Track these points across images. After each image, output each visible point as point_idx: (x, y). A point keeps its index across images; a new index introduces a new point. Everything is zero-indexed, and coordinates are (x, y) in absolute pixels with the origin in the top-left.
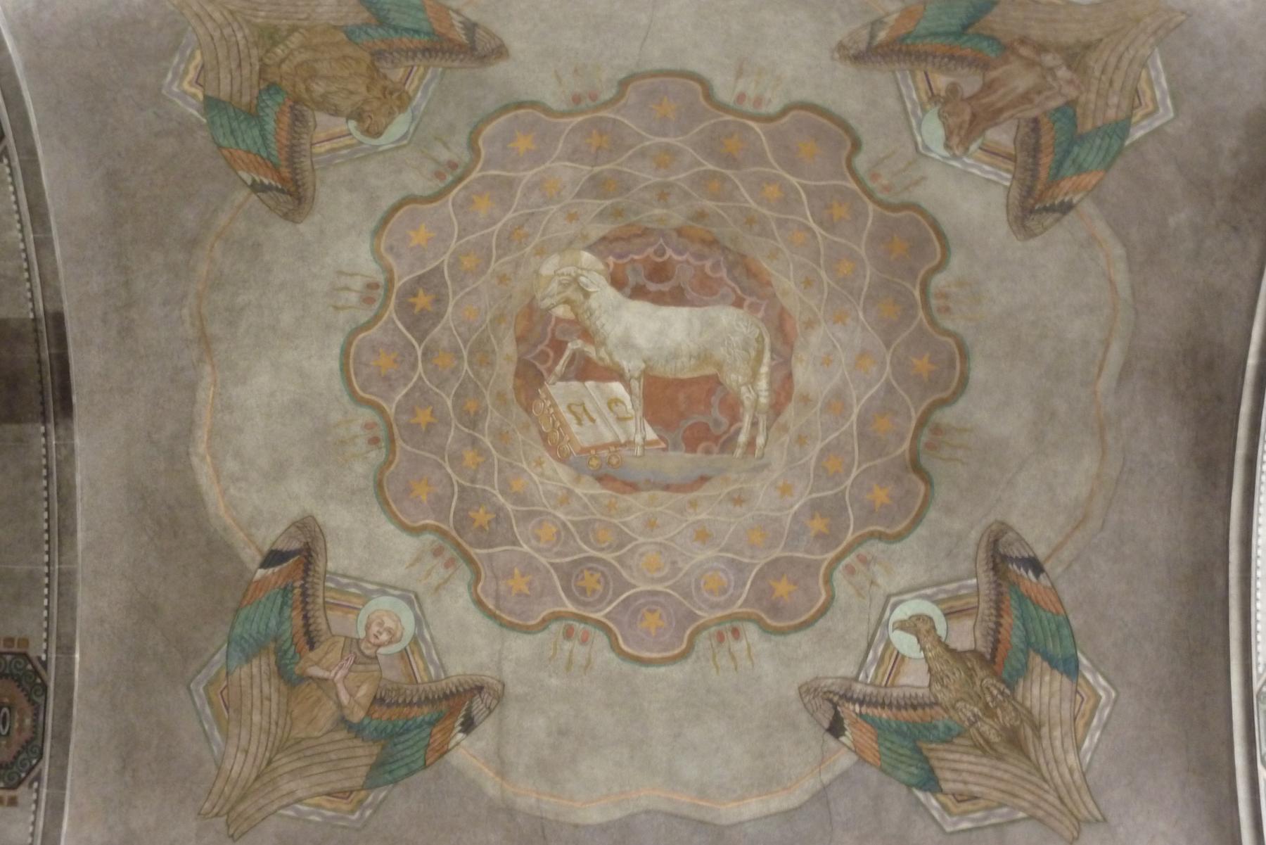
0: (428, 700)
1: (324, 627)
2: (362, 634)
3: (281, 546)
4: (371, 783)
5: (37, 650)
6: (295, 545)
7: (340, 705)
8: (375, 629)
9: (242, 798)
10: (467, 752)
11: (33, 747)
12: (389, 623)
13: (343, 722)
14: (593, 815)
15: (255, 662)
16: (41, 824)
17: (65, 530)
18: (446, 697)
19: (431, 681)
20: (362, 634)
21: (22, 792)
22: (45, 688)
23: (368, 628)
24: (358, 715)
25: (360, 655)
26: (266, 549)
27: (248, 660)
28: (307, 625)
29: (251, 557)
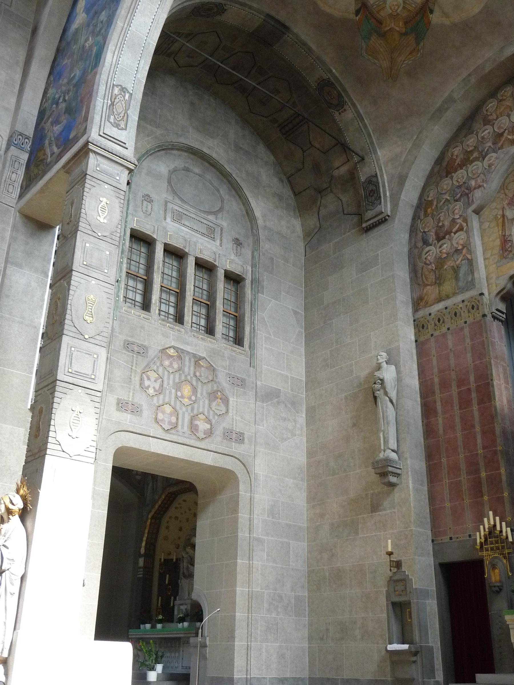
0: (417, 14)
1: (380, 17)
2: (391, 11)
3: (357, 8)
4: (418, 44)
5: (325, 77)
6: (360, 5)
7: (397, 31)
8: (393, 8)
9: (391, 72)
10: (435, 18)
11: (340, 96)
12: (395, 3)
13: (402, 34)
14: (477, 10)
15: (372, 38)
16: (353, 111)
17: (310, 49)
18: (421, 9)
19: (415, 8)
20: (391, 11)
21: (345, 107)
22: (333, 83)
23: (391, 9)
24: (404, 30)
25: (394, 16)
26: (354, 12)
27: (370, 39)
28: (377, 20)
29: (352, 16)
